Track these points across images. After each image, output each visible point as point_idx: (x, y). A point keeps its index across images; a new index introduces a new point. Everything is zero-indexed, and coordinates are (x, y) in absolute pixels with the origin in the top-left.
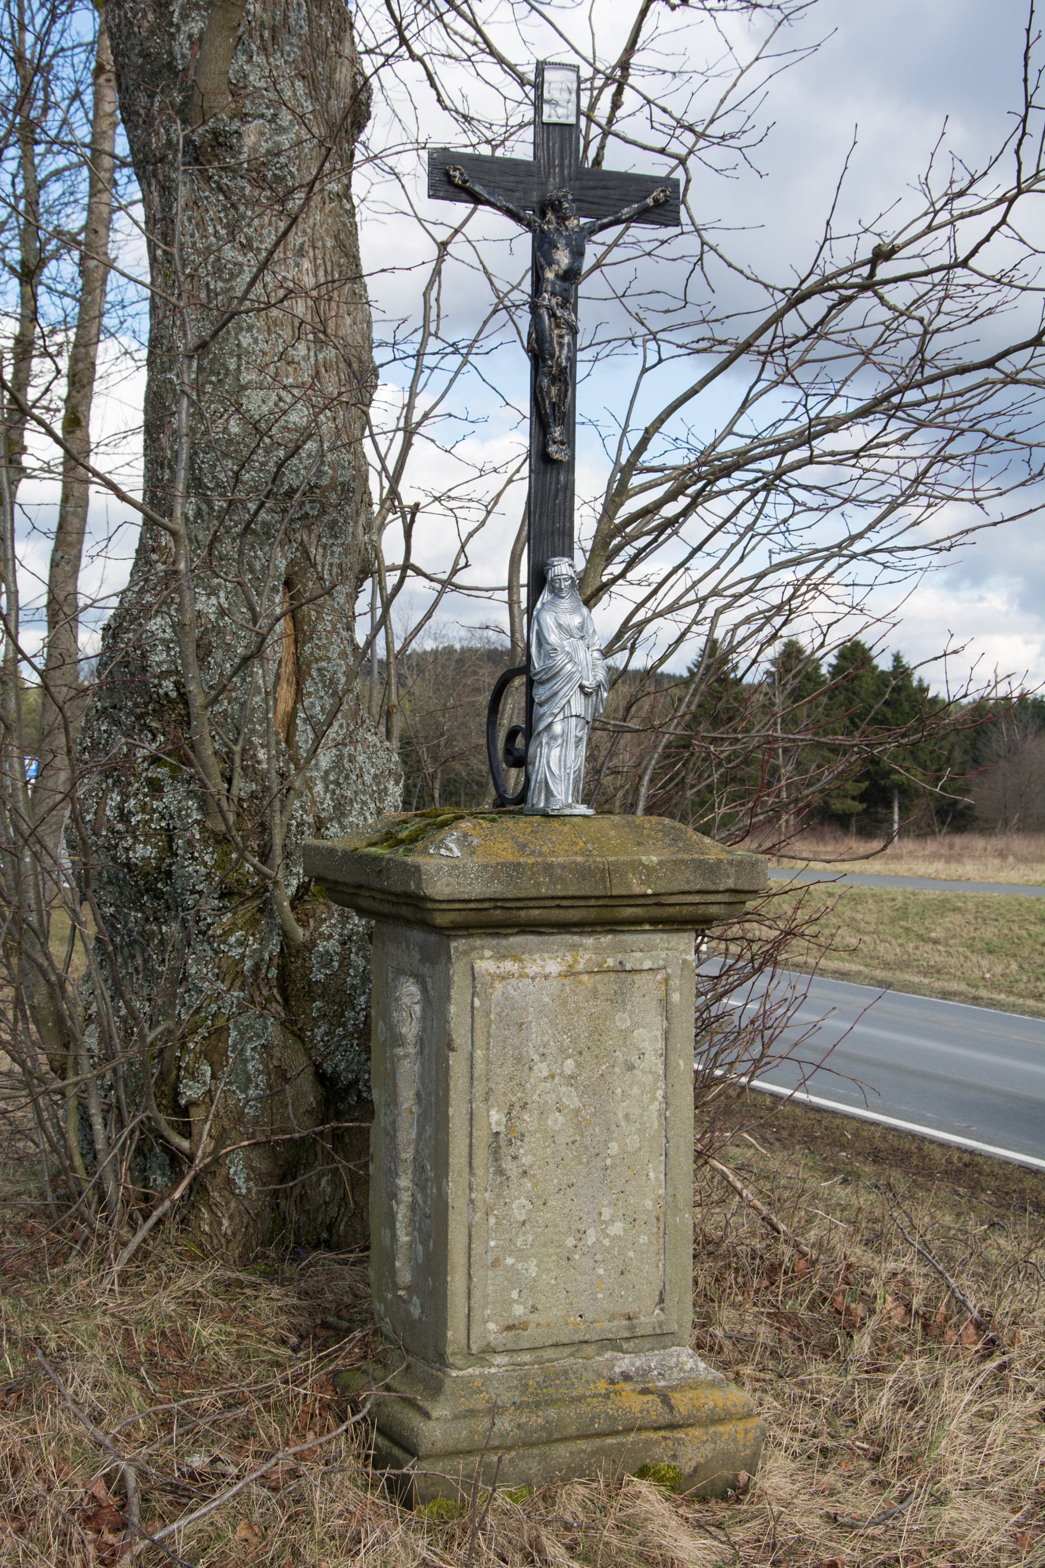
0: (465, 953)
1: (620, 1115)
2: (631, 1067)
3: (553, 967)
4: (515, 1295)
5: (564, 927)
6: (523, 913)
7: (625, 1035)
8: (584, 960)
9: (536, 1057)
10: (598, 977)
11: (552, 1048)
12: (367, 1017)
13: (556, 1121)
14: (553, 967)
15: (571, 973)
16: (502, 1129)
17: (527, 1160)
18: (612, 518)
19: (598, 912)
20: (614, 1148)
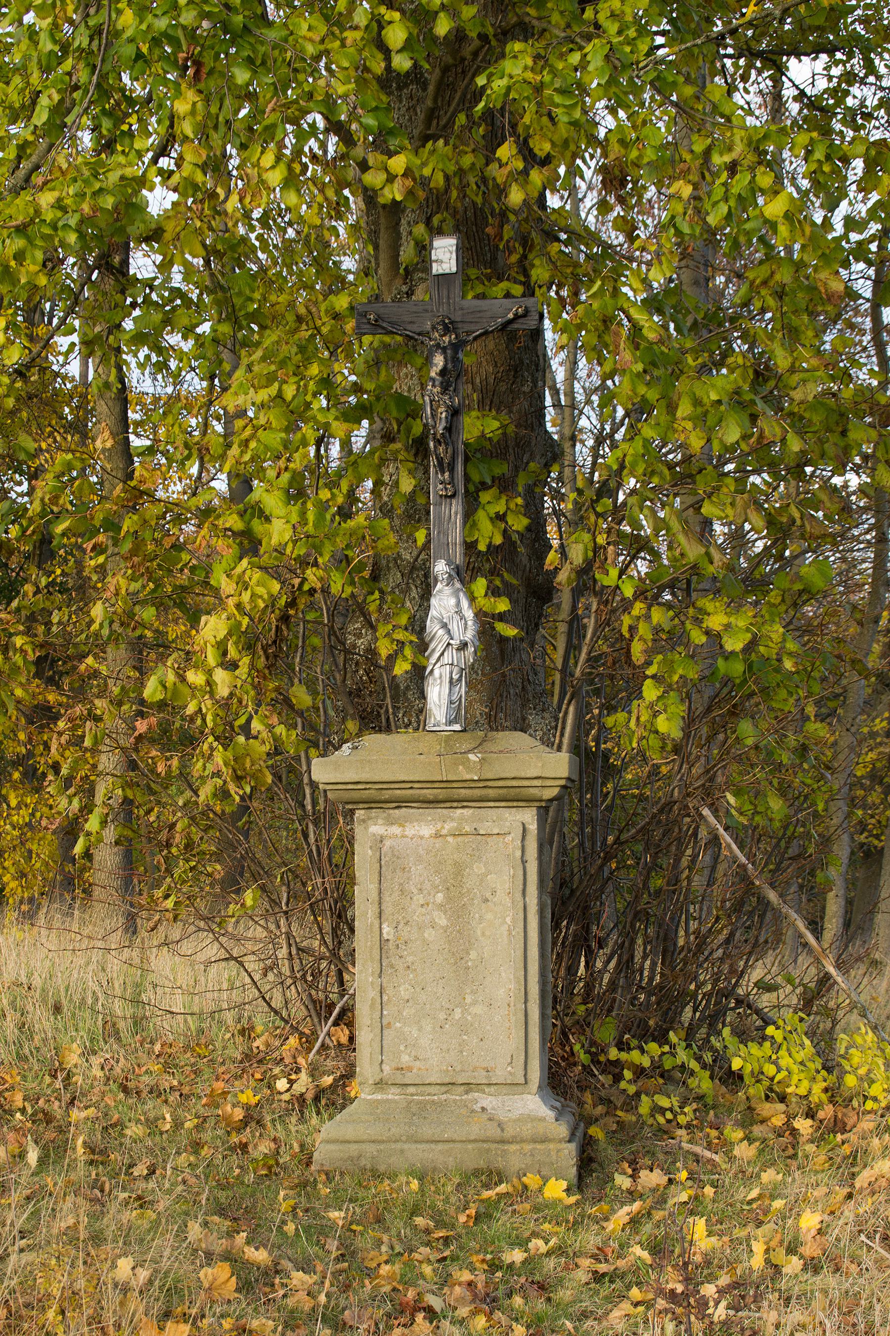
0: (364, 821)
1: (479, 933)
2: (486, 900)
3: (427, 831)
4: (402, 1048)
5: (434, 802)
6: (532, 790)
7: (482, 878)
8: (448, 826)
9: (415, 891)
10: (460, 839)
11: (427, 885)
12: (428, 126)
13: (429, 934)
14: (427, 831)
15: (438, 835)
16: (391, 937)
17: (410, 959)
18: (550, 388)
19: (441, 797)
20: (473, 955)
